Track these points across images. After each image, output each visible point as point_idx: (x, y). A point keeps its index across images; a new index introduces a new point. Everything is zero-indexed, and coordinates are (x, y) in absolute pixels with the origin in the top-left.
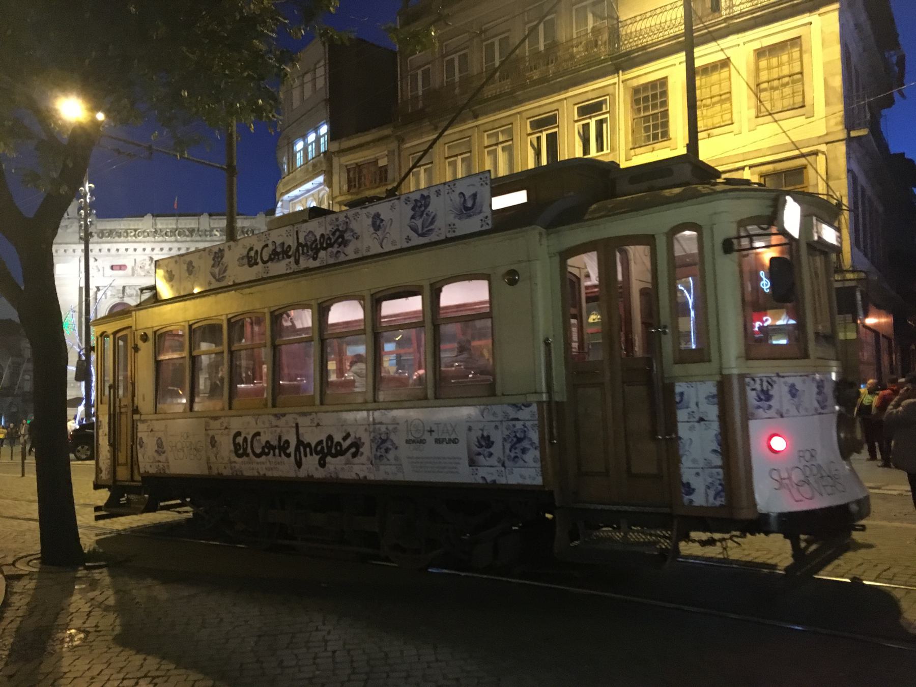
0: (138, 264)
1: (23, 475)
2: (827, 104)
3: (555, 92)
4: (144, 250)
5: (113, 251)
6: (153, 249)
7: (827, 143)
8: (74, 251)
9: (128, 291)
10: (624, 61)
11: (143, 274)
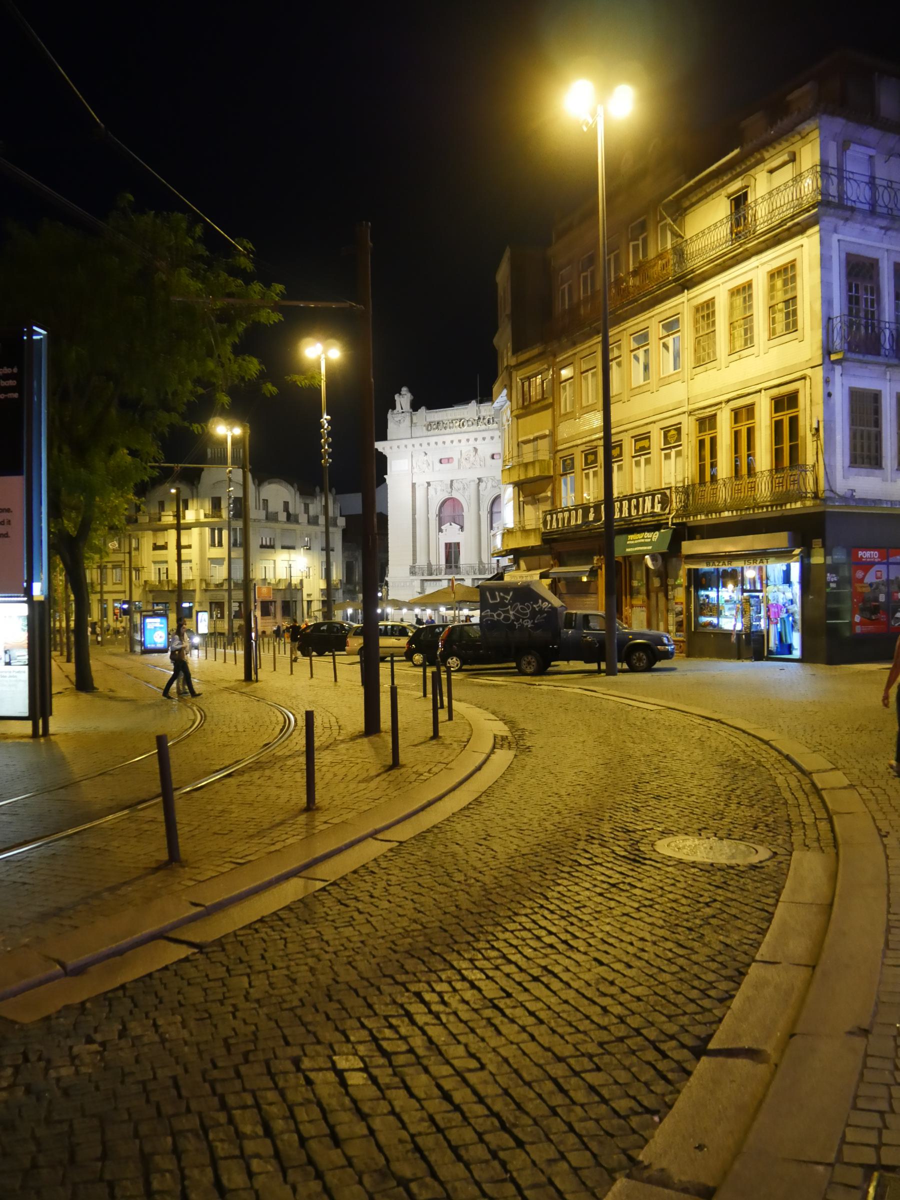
0: (464, 456)
1: (292, 673)
2: (812, 329)
3: (645, 311)
4: (468, 440)
5: (440, 443)
6: (476, 439)
7: (812, 367)
8: (406, 446)
9: (455, 485)
10: (686, 283)
11: (468, 466)
